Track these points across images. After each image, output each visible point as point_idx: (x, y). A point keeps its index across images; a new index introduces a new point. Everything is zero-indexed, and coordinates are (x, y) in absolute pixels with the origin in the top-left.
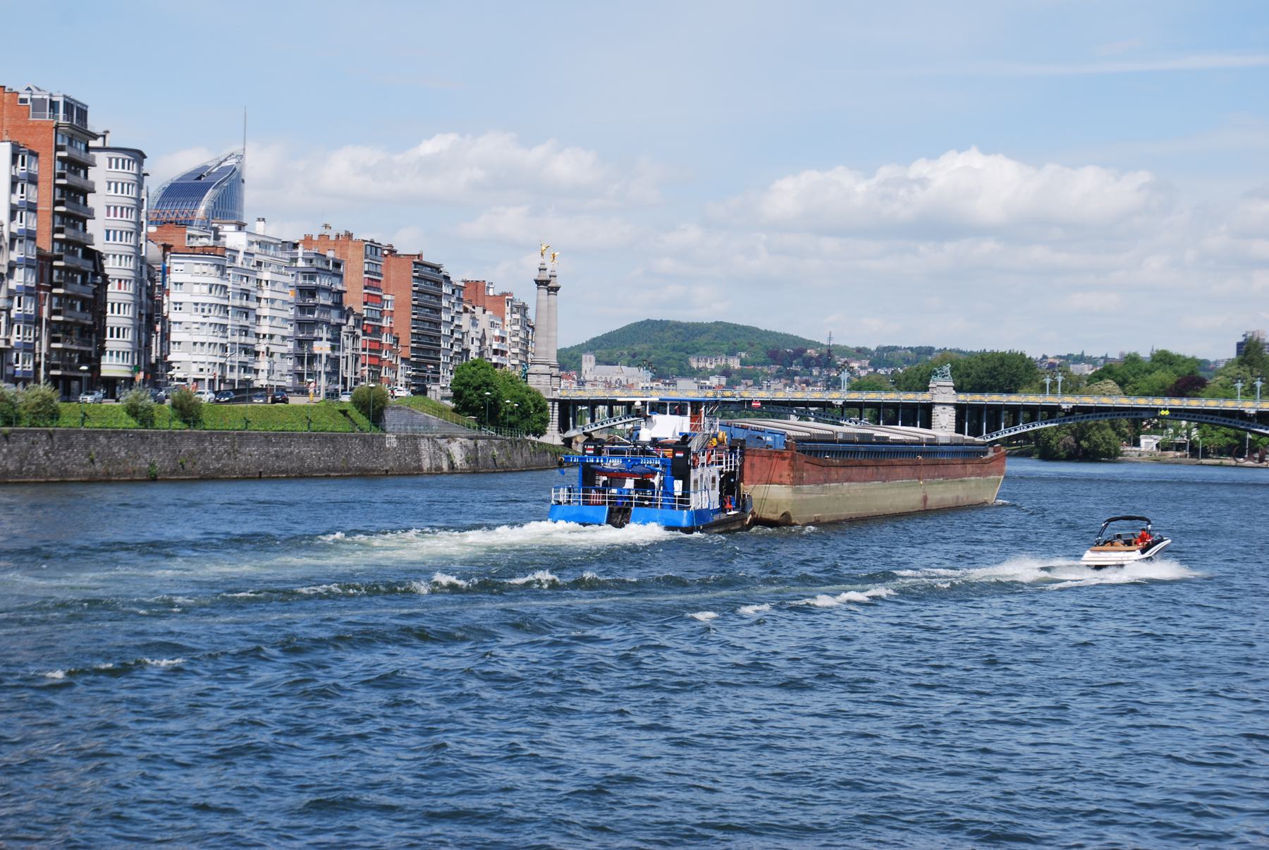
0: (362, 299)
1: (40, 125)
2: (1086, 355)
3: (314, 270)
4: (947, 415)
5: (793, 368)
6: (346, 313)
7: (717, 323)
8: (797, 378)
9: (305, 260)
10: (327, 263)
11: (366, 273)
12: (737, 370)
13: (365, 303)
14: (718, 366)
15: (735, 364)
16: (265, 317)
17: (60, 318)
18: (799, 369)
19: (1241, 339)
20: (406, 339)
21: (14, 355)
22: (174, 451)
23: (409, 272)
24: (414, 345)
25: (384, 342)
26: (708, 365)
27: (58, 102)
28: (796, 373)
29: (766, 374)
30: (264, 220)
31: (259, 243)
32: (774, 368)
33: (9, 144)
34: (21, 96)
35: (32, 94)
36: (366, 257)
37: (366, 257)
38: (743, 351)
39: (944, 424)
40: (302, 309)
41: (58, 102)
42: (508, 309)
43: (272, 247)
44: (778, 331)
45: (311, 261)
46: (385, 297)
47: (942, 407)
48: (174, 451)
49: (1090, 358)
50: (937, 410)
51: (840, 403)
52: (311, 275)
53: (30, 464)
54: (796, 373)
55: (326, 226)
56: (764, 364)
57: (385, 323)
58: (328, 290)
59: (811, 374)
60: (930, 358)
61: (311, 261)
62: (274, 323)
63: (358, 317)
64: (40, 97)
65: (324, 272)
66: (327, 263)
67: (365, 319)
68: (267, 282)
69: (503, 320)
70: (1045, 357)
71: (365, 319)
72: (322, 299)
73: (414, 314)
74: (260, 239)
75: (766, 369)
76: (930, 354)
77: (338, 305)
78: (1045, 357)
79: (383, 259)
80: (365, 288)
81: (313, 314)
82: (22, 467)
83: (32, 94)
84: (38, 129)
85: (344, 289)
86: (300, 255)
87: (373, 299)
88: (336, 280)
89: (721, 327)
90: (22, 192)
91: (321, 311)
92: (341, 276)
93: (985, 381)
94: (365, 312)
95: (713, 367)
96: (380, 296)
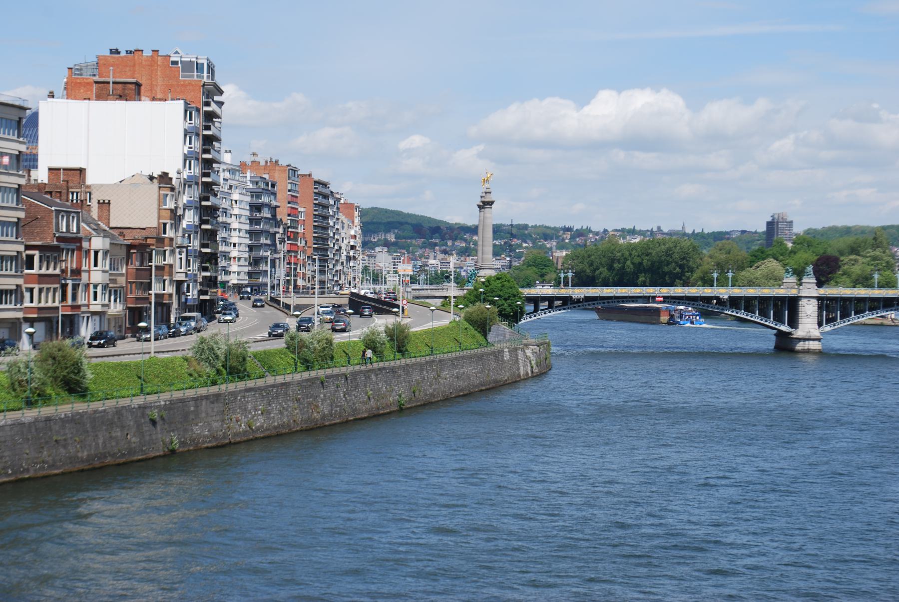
0: (287, 211)
1: (190, 84)
2: (636, 228)
3: (260, 191)
4: (811, 306)
5: (434, 240)
6: (278, 223)
7: (373, 208)
8: (437, 248)
9: (252, 182)
10: (267, 184)
11: (289, 191)
12: (394, 242)
13: (289, 215)
14: (379, 240)
15: (391, 238)
16: (235, 230)
17: (208, 250)
18: (437, 241)
19: (770, 219)
20: (311, 241)
21: (186, 284)
22: (409, 382)
23: (311, 190)
24: (316, 246)
25: (299, 244)
26: (372, 239)
27: (203, 64)
28: (436, 245)
29: (415, 245)
30: (230, 151)
31: (228, 170)
32: (420, 241)
33: (182, 102)
34: (172, 59)
35: (181, 57)
36: (289, 178)
37: (289, 178)
38: (396, 229)
39: (809, 313)
40: (252, 221)
41: (203, 64)
42: (356, 214)
43: (237, 173)
44: (417, 214)
45: (257, 183)
46: (300, 209)
47: (807, 300)
48: (409, 382)
49: (640, 231)
50: (803, 302)
51: (726, 297)
52: (258, 195)
53: (337, 406)
54: (436, 245)
55: (254, 154)
56: (411, 238)
57: (300, 230)
58: (268, 206)
59: (446, 245)
60: (526, 232)
61: (257, 183)
62: (241, 234)
63: (285, 226)
64: (189, 60)
65: (265, 191)
66: (267, 184)
67: (289, 227)
68: (236, 201)
69: (353, 222)
70: (605, 231)
71: (289, 227)
72: (266, 214)
73: (315, 222)
74: (230, 167)
75: (414, 241)
76: (527, 230)
77: (274, 216)
78: (605, 231)
79: (299, 180)
80: (289, 203)
81: (259, 225)
82: (332, 410)
83: (181, 57)
84: (188, 88)
85: (278, 204)
86: (249, 178)
87: (293, 212)
88: (272, 197)
89: (376, 211)
90: (190, 143)
91: (265, 223)
92: (274, 194)
93: (663, 258)
94: (289, 222)
95: (376, 240)
96: (297, 209)
